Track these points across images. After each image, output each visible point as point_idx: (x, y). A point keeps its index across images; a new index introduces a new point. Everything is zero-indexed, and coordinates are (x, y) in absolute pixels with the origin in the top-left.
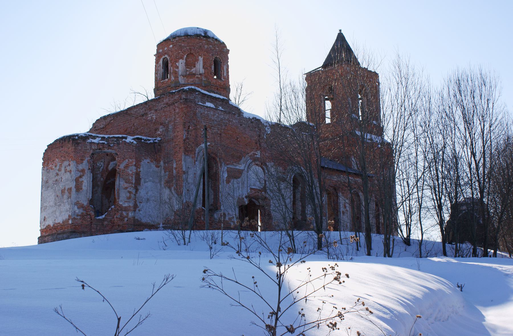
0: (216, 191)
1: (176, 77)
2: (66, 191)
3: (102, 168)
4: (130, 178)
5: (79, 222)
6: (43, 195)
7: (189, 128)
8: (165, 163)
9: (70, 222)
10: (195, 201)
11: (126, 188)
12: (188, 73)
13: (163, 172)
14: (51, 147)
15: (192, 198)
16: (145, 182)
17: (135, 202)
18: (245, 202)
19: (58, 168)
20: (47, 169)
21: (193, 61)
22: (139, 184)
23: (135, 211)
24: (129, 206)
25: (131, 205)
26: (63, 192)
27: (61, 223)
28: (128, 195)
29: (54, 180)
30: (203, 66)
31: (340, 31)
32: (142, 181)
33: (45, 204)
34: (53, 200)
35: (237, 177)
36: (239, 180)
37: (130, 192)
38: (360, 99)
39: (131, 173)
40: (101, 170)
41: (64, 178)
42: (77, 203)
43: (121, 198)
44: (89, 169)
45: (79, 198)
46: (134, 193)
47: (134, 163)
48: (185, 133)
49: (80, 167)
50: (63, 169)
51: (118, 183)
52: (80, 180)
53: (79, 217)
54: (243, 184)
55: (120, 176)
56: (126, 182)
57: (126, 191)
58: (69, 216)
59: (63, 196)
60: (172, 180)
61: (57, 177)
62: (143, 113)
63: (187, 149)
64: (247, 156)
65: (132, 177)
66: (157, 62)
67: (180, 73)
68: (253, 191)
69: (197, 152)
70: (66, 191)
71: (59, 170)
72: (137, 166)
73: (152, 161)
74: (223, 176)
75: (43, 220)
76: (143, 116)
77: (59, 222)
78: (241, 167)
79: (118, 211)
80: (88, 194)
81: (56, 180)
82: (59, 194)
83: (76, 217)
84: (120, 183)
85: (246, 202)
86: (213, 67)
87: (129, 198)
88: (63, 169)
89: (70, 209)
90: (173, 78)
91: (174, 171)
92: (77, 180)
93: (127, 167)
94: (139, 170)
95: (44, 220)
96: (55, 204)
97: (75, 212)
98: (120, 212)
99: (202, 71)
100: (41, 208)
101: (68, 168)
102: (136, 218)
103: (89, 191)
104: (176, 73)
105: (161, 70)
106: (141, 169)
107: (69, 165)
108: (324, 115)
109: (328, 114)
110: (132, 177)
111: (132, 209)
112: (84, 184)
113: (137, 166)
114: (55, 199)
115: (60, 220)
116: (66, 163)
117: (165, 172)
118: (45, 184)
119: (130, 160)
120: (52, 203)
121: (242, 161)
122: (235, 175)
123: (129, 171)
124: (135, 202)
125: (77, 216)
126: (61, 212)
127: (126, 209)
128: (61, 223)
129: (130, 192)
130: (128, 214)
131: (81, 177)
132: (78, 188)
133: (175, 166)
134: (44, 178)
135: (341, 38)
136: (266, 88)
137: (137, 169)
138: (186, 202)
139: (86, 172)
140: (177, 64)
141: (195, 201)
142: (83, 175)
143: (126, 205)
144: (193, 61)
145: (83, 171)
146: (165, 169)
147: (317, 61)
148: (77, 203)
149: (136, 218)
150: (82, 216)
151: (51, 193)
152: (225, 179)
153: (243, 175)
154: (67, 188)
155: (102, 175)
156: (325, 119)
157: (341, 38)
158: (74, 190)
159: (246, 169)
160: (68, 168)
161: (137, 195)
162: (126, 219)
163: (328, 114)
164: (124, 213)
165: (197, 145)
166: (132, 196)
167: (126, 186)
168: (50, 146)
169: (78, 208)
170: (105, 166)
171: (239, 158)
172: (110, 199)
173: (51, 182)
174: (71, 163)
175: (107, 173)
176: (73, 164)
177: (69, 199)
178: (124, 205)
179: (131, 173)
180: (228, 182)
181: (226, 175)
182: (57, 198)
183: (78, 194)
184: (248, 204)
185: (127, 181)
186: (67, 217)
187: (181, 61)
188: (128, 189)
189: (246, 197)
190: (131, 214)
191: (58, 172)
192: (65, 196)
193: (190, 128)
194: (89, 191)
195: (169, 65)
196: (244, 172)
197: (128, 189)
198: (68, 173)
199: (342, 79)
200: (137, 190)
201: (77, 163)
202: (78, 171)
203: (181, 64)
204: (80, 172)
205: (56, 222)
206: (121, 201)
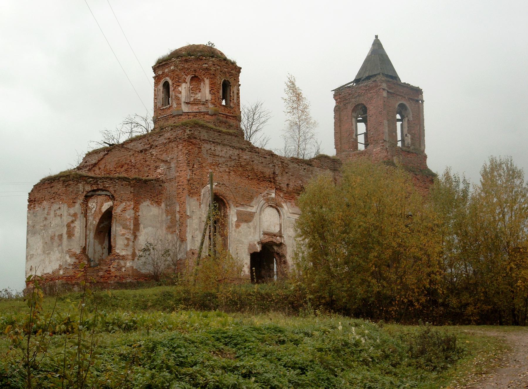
0: (225, 237)
1: (179, 104)
2: (56, 238)
3: (94, 209)
4: (128, 223)
5: (71, 273)
6: (29, 241)
7: (193, 167)
8: (166, 206)
9: (61, 272)
10: (201, 248)
11: (123, 235)
12: (192, 99)
13: (164, 216)
14: (38, 188)
15: (198, 244)
16: (144, 228)
17: (134, 250)
18: (257, 249)
19: (46, 211)
20: (34, 213)
21: (199, 77)
22: (138, 230)
23: (133, 260)
24: (127, 255)
25: (130, 253)
26: (52, 238)
27: (51, 273)
28: (126, 242)
29: (42, 224)
30: (210, 91)
31: (377, 37)
32: (141, 226)
33: (31, 253)
34: (41, 247)
35: (247, 221)
36: (251, 224)
37: (128, 239)
38: (399, 120)
39: (129, 217)
40: (93, 211)
41: (53, 223)
42: (69, 251)
43: (118, 246)
44: (82, 213)
45: (71, 245)
46: (133, 240)
47: (132, 207)
48: (190, 173)
49: (72, 211)
50: (52, 213)
51: (114, 229)
52: (72, 225)
53: (71, 267)
54: (255, 228)
55: (116, 221)
56: (123, 228)
57: (124, 237)
58: (60, 266)
59: (52, 243)
60: (175, 225)
61: (45, 222)
62: (141, 149)
63: (192, 191)
64: (260, 196)
65: (130, 222)
66: (156, 84)
67: (183, 100)
68: (266, 236)
69: (202, 194)
70: (56, 238)
71: (48, 214)
72: (136, 209)
73: (152, 204)
74: (232, 220)
75: (29, 270)
76: (141, 151)
77: (48, 272)
78: (253, 210)
79: (114, 259)
80: (81, 241)
81: (45, 225)
82: (48, 240)
83: (68, 267)
84: (117, 229)
85: (259, 248)
86: (221, 91)
87: (127, 245)
88: (52, 213)
89: (61, 258)
90: (175, 105)
91: (178, 216)
92: (68, 226)
93: (124, 210)
94: (137, 214)
95: (31, 270)
96: (44, 252)
97: (66, 261)
98: (117, 261)
99: (208, 97)
100: (27, 257)
101: (58, 212)
102: (135, 268)
103: (82, 238)
104: (178, 99)
105: (161, 95)
106: (140, 213)
107: (60, 208)
108: (356, 140)
109: (361, 139)
110: (130, 222)
111: (130, 257)
112: (76, 230)
113: (136, 209)
114: (43, 247)
115: (49, 269)
116: (56, 206)
117: (167, 216)
118: (31, 230)
119: (128, 203)
120: (39, 251)
121: (254, 202)
122: (245, 218)
123: (127, 215)
124: (134, 250)
125: (69, 265)
126: (50, 262)
127: (124, 258)
128: (51, 273)
129: (128, 239)
130: (126, 263)
131: (73, 222)
132: (70, 234)
133: (178, 209)
134: (30, 222)
135: (377, 48)
136: (287, 104)
137: (135, 213)
138: (191, 250)
139: (79, 216)
140: (180, 88)
141: (201, 248)
142: (75, 220)
143: (123, 253)
144: (199, 77)
145: (75, 215)
146: (167, 212)
147: (348, 74)
148: (69, 251)
149: (135, 268)
150: (75, 265)
151: (39, 240)
152: (234, 224)
153: (255, 218)
154: (57, 234)
155: (94, 218)
156: (357, 146)
157: (377, 48)
158: (65, 236)
159: (258, 212)
160: (58, 212)
161: (135, 242)
162: (124, 269)
163: (361, 139)
164: (122, 263)
165: (203, 185)
166: (131, 243)
167: (123, 232)
168: (35, 186)
169: (70, 257)
170: (98, 207)
171: (251, 198)
172: (104, 245)
173: (38, 227)
174: (62, 206)
175: (100, 216)
176: (64, 207)
177: (60, 247)
178: (121, 254)
179: (129, 217)
180: (237, 226)
181: (235, 219)
182: (45, 246)
183: (69, 241)
184: (261, 251)
185: (125, 227)
186: (58, 267)
187: (184, 85)
188: (126, 236)
189: (259, 243)
190: (129, 264)
191: (46, 216)
192: (55, 244)
193: (195, 166)
194: (82, 238)
195: (171, 89)
196: (256, 214)
197: (126, 236)
198: (59, 218)
199: (378, 94)
200: (135, 237)
201: (69, 207)
202: (70, 215)
203: (184, 88)
204: (72, 216)
205: (45, 272)
206: (118, 249)
